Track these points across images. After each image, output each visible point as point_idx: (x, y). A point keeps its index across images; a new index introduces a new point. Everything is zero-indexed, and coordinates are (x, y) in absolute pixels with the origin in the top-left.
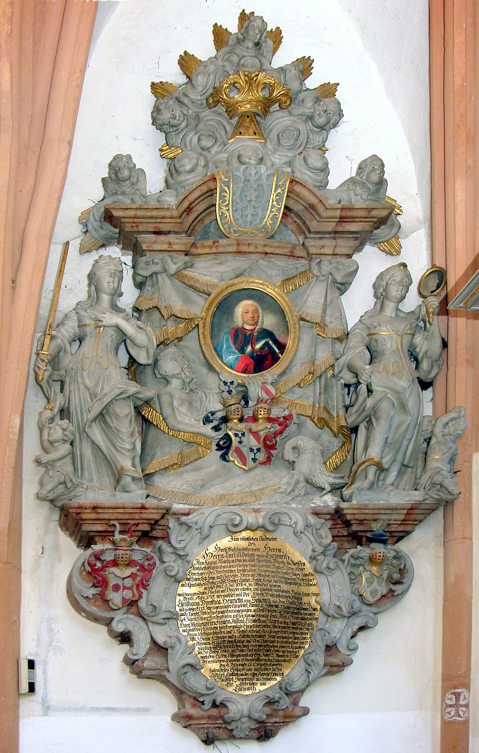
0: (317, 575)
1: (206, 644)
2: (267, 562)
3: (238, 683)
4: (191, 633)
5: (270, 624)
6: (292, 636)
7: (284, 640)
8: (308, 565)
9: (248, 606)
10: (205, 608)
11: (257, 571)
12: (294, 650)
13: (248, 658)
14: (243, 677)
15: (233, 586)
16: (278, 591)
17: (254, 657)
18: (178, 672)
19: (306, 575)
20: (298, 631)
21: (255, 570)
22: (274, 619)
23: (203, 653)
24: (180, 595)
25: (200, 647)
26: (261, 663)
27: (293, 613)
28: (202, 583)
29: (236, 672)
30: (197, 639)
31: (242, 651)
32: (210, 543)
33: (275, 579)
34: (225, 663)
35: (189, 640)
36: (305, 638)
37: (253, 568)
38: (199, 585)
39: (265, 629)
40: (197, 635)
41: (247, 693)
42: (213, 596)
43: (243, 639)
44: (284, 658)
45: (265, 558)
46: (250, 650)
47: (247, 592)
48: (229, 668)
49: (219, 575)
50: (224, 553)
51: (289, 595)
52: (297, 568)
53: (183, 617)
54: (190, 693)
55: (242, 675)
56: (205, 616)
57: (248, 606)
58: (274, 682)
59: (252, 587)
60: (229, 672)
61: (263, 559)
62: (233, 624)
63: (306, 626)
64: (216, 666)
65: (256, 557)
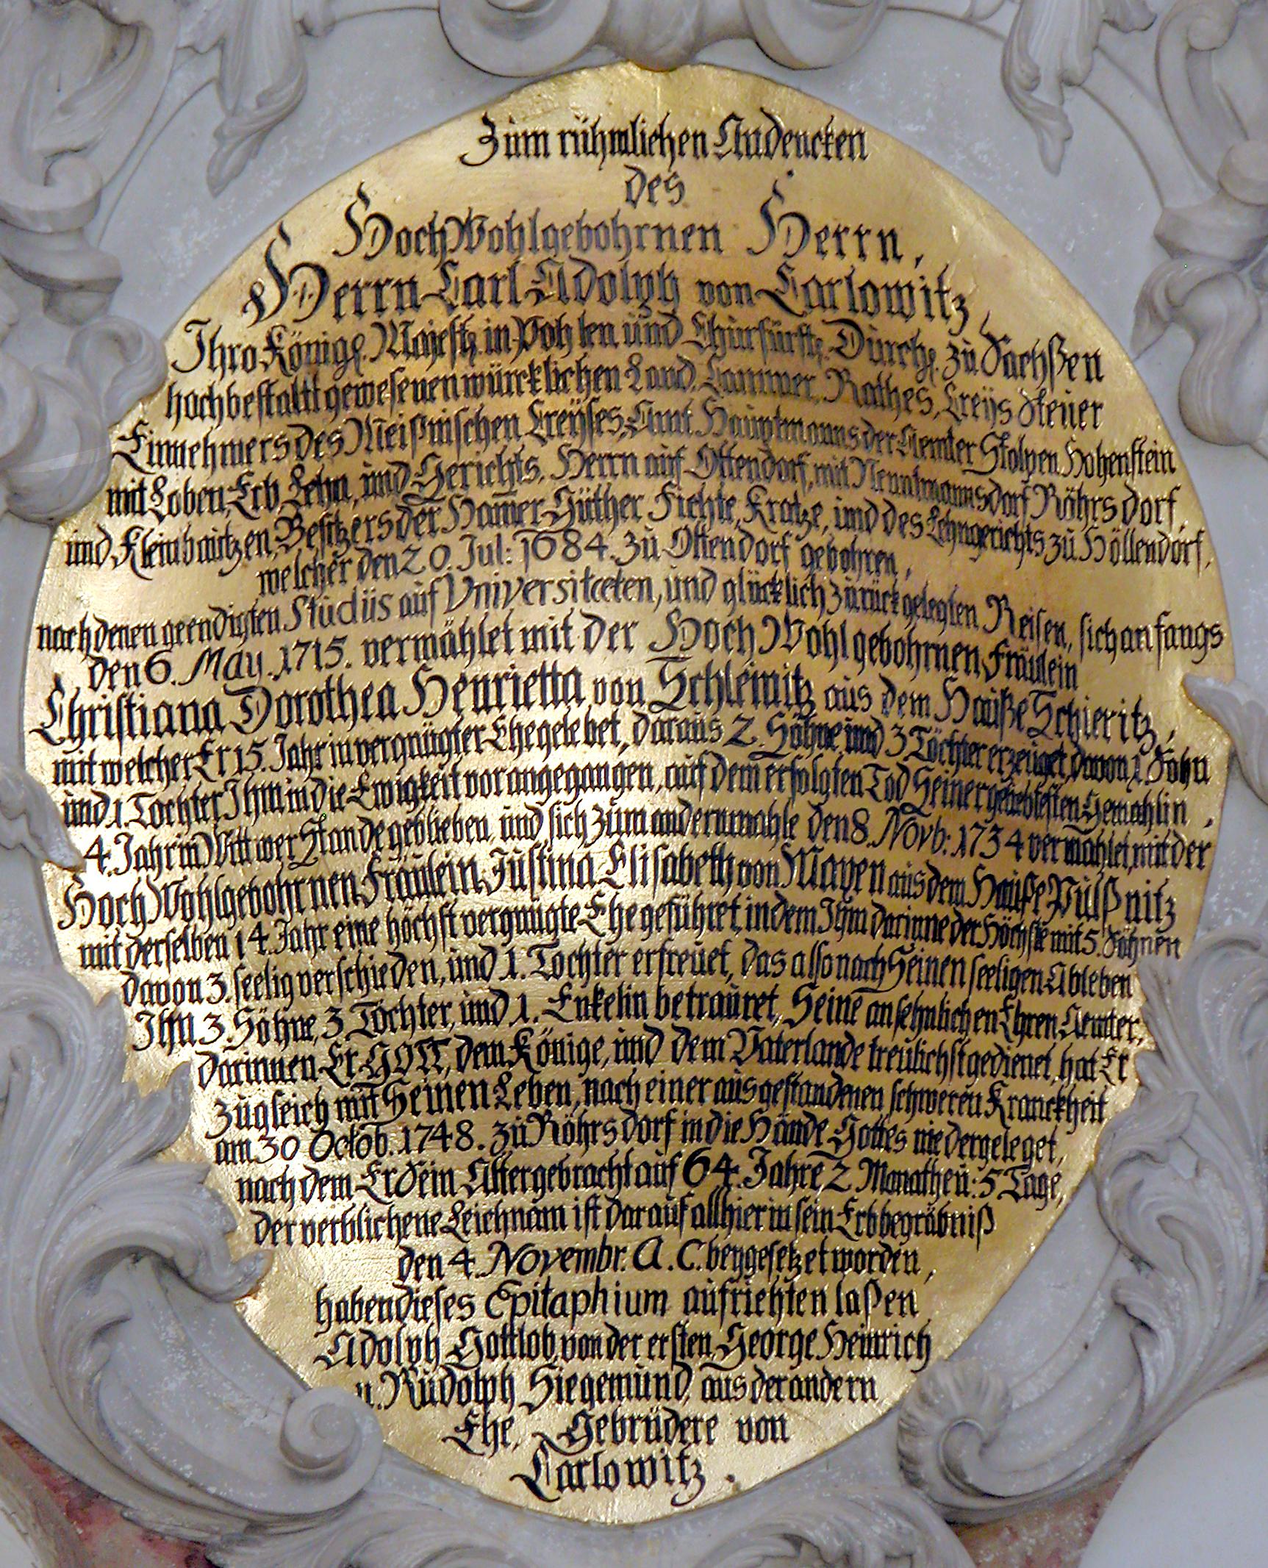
0: (1191, 458)
1: (276, 1071)
2: (780, 342)
3: (554, 1418)
4: (156, 974)
5: (811, 897)
6: (993, 1000)
7: (933, 1039)
8: (1124, 378)
9: (624, 734)
10: (272, 753)
11: (699, 421)
12: (1019, 1129)
13: (632, 1196)
14: (596, 1367)
15: (493, 554)
16: (875, 601)
17: (679, 1188)
18: (47, 1319)
19: (1108, 465)
20: (1044, 960)
21: (677, 421)
22: (842, 850)
23: (257, 1149)
24: (55, 639)
25: (230, 1097)
26: (742, 1239)
27: (1000, 797)
28: (241, 529)
29: (533, 1323)
30: (202, 1029)
31: (585, 1132)
32: (305, 179)
33: (854, 499)
34: (441, 1245)
35: (139, 1033)
36: (1100, 1026)
37: (666, 401)
38: (215, 548)
39: (769, 940)
40: (209, 989)
41: (627, 1505)
42: (337, 645)
43: (587, 1029)
44: (954, 1173)
45: (766, 307)
46: (648, 1129)
47: (610, 611)
48: (479, 1289)
49: (380, 462)
50: (424, 269)
51: (970, 637)
52: (1035, 404)
53: (82, 837)
54: (151, 1512)
55: (587, 1346)
56: (273, 824)
57: (624, 734)
58: (852, 1416)
59: (658, 571)
60: (480, 1320)
61: (746, 316)
62: (505, 898)
63: (1116, 918)
64: (368, 1268)
65: (689, 304)
